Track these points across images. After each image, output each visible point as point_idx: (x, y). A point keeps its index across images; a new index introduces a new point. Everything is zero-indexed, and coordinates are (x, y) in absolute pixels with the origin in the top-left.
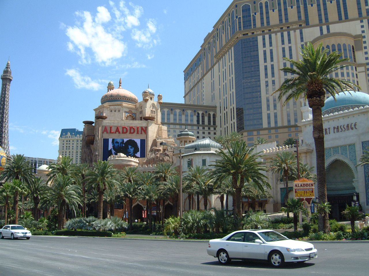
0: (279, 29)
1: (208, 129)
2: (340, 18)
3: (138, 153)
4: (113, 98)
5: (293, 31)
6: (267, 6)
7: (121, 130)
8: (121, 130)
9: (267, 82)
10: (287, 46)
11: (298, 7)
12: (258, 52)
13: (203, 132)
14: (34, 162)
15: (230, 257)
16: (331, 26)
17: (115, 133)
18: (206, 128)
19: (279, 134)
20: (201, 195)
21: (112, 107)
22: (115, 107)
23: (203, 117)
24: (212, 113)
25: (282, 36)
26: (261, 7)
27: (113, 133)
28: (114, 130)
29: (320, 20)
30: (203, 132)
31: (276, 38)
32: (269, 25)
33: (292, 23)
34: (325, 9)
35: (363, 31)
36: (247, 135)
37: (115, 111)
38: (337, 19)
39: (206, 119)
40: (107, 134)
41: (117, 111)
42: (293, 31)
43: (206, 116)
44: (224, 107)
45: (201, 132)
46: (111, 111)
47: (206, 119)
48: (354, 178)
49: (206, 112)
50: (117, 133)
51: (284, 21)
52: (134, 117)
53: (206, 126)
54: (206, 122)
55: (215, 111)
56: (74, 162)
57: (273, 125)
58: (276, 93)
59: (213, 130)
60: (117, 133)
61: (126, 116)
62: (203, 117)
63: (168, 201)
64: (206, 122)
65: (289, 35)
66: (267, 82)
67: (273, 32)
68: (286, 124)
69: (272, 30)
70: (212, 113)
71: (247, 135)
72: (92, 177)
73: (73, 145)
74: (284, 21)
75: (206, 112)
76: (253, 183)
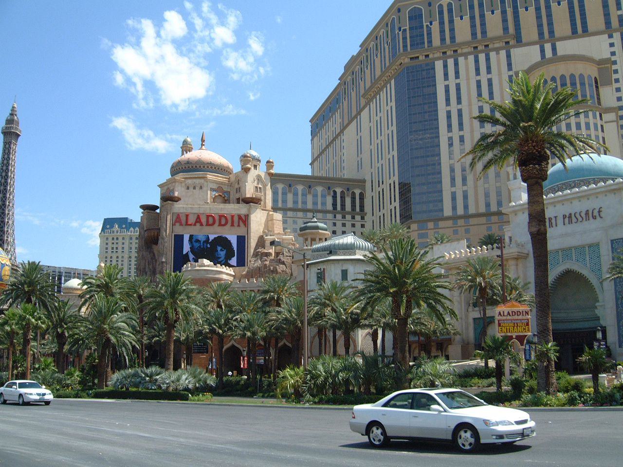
0: (471, 49)
1: (352, 219)
2: (574, 31)
3: (233, 258)
4: (190, 166)
5: (494, 53)
6: (450, 11)
7: (204, 220)
8: (204, 220)
9: (450, 139)
10: (484, 77)
11: (504, 12)
12: (436, 88)
13: (342, 223)
14: (57, 274)
15: (388, 435)
16: (558, 44)
17: (195, 225)
18: (348, 217)
19: (471, 227)
20: (340, 330)
21: (189, 181)
22: (194, 180)
23: (343, 198)
24: (357, 192)
25: (477, 61)
26: (441, 13)
27: (191, 225)
28: (192, 220)
29: (541, 34)
30: (342, 223)
31: (467, 64)
32: (455, 42)
33: (493, 39)
34: (549, 15)
35: (613, 52)
36: (417, 229)
37: (194, 188)
38: (569, 32)
39: (348, 201)
40: (181, 227)
41: (198, 188)
42: (495, 53)
43: (348, 196)
44: (379, 182)
45: (339, 224)
46: (188, 188)
47: (348, 201)
48: (598, 301)
49: (348, 190)
50: (198, 224)
51: (479, 35)
52: (226, 198)
53: (348, 213)
54: (348, 207)
55: (363, 188)
56: (125, 275)
57: (460, 211)
58: (466, 157)
59: (360, 220)
60: (198, 224)
61: (214, 196)
62: (343, 198)
63: (284, 339)
64: (348, 207)
65: (488, 59)
66: (450, 139)
67: (462, 55)
68: (482, 209)
69: (459, 51)
70: (357, 192)
71: (417, 229)
72: (156, 300)
73: (123, 246)
74: (479, 35)
75: (348, 190)
76: (428, 309)
